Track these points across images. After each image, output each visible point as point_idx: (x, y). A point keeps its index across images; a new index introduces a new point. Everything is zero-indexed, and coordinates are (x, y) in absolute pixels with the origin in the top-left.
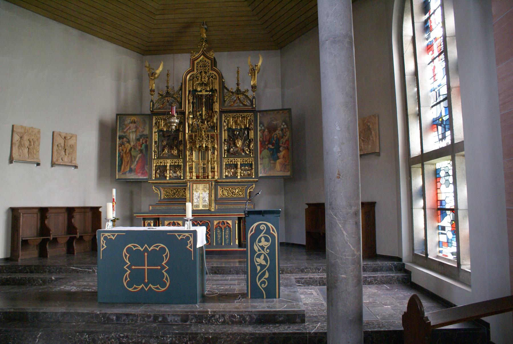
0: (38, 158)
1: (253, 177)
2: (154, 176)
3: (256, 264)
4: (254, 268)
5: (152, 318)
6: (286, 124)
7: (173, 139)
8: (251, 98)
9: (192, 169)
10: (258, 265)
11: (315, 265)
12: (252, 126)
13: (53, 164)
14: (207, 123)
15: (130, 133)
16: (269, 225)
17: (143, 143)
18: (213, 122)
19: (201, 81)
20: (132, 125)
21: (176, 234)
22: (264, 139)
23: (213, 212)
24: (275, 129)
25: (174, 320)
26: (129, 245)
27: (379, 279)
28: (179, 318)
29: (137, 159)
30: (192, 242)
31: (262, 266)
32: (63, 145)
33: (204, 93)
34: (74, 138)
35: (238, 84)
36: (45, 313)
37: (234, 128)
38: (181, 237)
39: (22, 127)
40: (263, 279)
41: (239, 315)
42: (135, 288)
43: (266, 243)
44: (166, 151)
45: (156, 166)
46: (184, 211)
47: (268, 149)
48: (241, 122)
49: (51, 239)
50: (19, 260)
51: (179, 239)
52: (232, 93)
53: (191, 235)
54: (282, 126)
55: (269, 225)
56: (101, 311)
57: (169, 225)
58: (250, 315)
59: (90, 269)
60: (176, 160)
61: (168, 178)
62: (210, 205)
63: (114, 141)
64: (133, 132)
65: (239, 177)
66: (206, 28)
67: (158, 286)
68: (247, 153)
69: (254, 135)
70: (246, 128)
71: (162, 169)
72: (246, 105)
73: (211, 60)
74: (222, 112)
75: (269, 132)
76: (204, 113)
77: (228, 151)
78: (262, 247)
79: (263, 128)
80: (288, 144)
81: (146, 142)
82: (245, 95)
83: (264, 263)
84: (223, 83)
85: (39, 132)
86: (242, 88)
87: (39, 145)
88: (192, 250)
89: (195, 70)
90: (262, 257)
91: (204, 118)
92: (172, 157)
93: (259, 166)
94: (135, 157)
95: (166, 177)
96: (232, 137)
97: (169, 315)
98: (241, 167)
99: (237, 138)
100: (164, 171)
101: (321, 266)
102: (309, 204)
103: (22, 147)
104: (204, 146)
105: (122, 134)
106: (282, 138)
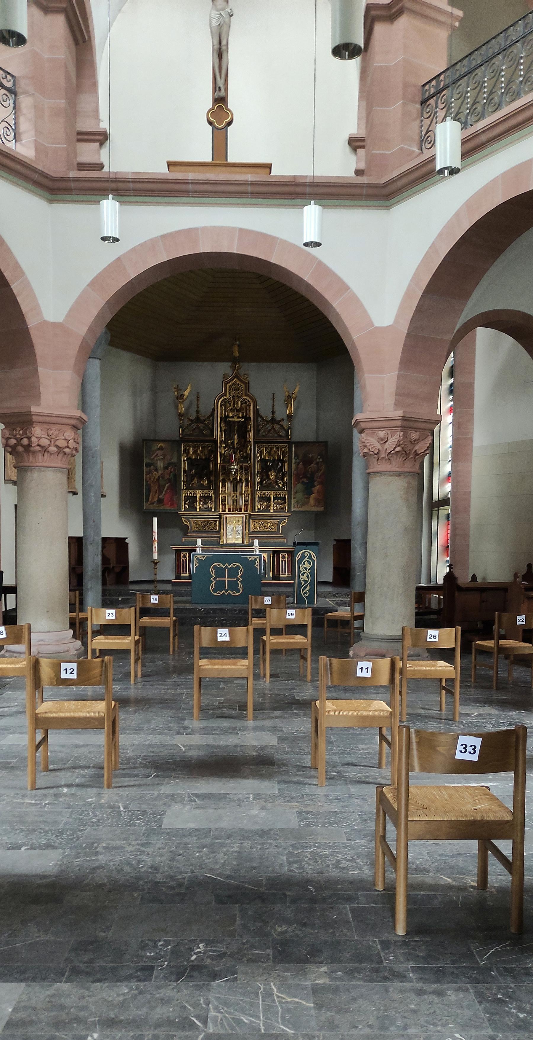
0: (75, 488)
4: (299, 582)
8: (286, 428)
12: (286, 458)
14: (239, 452)
15: (157, 460)
16: (311, 552)
17: (171, 472)
18: (246, 452)
19: (234, 406)
20: (160, 452)
29: (166, 488)
31: (305, 582)
33: (236, 419)
43: (309, 565)
44: (196, 480)
48: (275, 452)
52: (267, 421)
55: (311, 552)
60: (206, 491)
61: (198, 510)
63: (84, 447)
65: (272, 511)
68: (281, 486)
69: (288, 468)
70: (279, 460)
72: (281, 436)
74: (255, 442)
76: (236, 442)
77: (261, 483)
78: (306, 569)
79: (298, 461)
81: (175, 470)
82: (280, 425)
86: (278, 417)
89: (228, 394)
90: (306, 575)
91: (235, 446)
92: (201, 487)
93: (293, 500)
95: (196, 508)
102: (69, 537)
104: (238, 478)
105: (149, 461)
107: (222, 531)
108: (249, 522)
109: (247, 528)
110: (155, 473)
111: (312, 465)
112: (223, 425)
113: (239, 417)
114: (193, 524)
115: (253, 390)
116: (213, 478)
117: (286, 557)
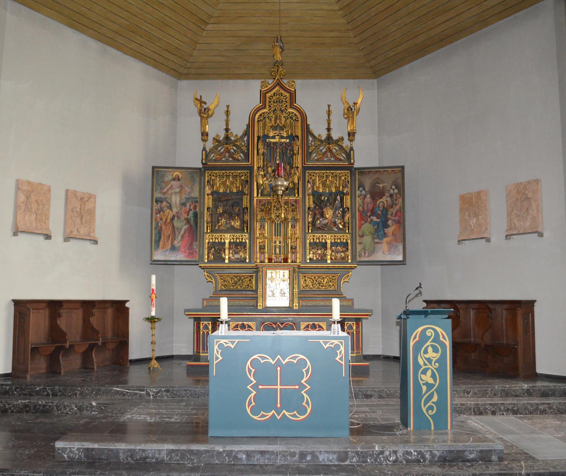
0: (48, 229)
1: (350, 261)
2: (206, 257)
3: (421, 382)
5: (297, 456)
6: (396, 187)
7: (233, 206)
9: (264, 249)
10: (423, 384)
11: (463, 387)
13: (67, 239)
16: (439, 329)
17: (190, 210)
21: (321, 341)
22: (366, 209)
23: (260, 310)
24: (381, 194)
25: (328, 458)
26: (255, 357)
27: (555, 407)
28: (335, 456)
29: (182, 233)
30: (343, 352)
32: (78, 209)
34: (92, 200)
35: (329, 129)
36: (144, 451)
37: (321, 191)
38: (328, 345)
39: (29, 183)
40: (430, 404)
41: (416, 451)
42: (263, 416)
43: (434, 355)
45: (208, 243)
46: (330, 308)
47: (370, 223)
49: (67, 347)
50: (28, 378)
51: (325, 347)
52: (321, 141)
53: (341, 343)
55: (439, 329)
56: (225, 447)
57: (307, 328)
58: (431, 451)
59: (143, 390)
60: (238, 235)
61: (227, 261)
62: (292, 301)
64: (176, 193)
65: (329, 261)
66: (281, 47)
67: (295, 412)
68: (341, 227)
73: (290, 93)
74: (305, 169)
77: (313, 223)
78: (429, 360)
79: (363, 193)
81: (195, 208)
82: (339, 145)
83: (431, 381)
84: (308, 126)
85: (49, 190)
87: (49, 210)
88: (343, 363)
89: (267, 106)
90: (429, 373)
92: (232, 230)
94: (179, 229)
95: (224, 259)
96: (320, 203)
97: (320, 452)
98: (331, 247)
99: (326, 206)
100: (221, 250)
101: (472, 388)
103: (30, 212)
106: (392, 207)
107: (260, 290)
108: (299, 276)
109: (296, 286)
110: (168, 210)
111: (384, 199)
112: (260, 146)
113: (282, 137)
114: (220, 281)
115: (300, 102)
116: (247, 217)
117: (354, 328)
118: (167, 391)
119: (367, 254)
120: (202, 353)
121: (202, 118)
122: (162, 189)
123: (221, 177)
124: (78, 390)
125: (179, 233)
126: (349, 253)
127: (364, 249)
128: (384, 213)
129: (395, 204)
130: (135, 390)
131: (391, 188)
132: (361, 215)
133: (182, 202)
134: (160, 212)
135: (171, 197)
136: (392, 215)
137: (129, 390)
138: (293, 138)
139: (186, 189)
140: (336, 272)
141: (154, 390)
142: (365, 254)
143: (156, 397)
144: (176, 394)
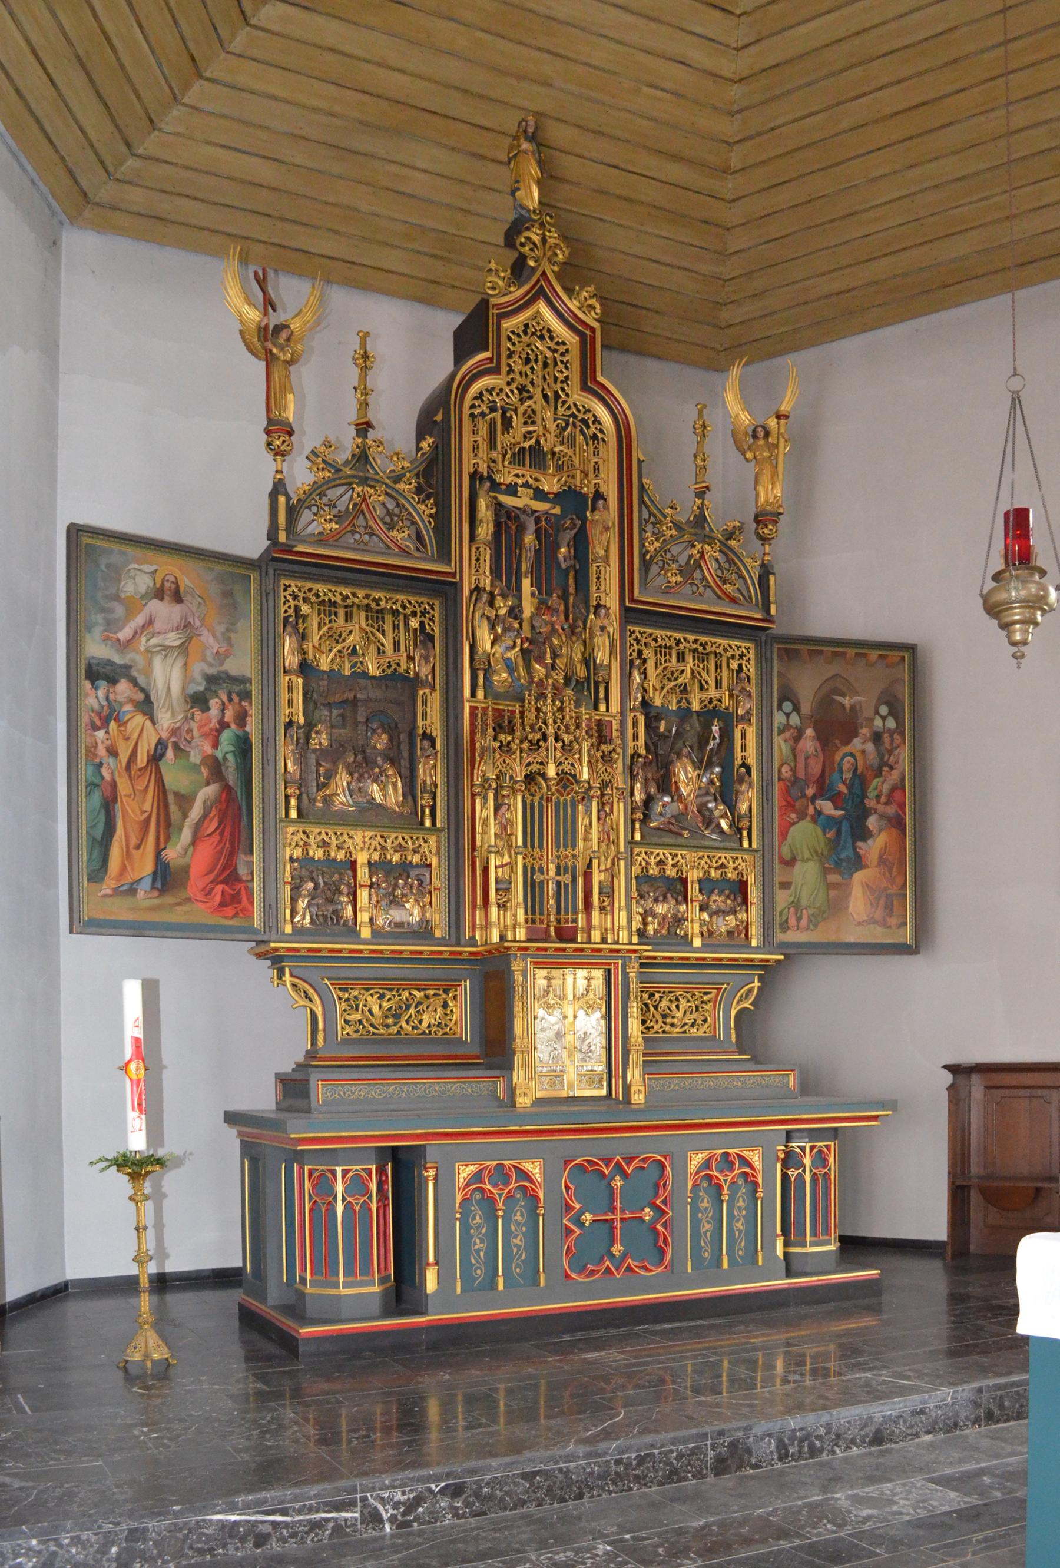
1: (754, 943)
17: (224, 725)
20: (164, 611)
22: (801, 774)
29: (196, 812)
44: (343, 779)
47: (814, 820)
54: (878, 722)
59: (349, 1505)
65: (697, 942)
70: (711, 712)
71: (330, 880)
75: (824, 739)
80: (902, 806)
81: (242, 718)
89: (504, 369)
92: (369, 815)
94: (185, 801)
104: (551, 771)
106: (878, 773)
110: (139, 719)
118: (456, 1491)
119: (804, 922)
120: (347, 1285)
121: (270, 359)
122: (111, 625)
123: (328, 607)
124: (30, 1552)
125: (185, 816)
126: (754, 912)
127: (796, 904)
128: (857, 790)
129: (887, 764)
130: (310, 1510)
131: (877, 712)
132: (786, 792)
133: (193, 688)
134: (105, 722)
135: (150, 663)
136: (878, 797)
137: (284, 1512)
138: (576, 502)
139: (207, 638)
140: (718, 979)
141: (399, 1497)
142: (799, 919)
143: (407, 1524)
144: (490, 1497)
